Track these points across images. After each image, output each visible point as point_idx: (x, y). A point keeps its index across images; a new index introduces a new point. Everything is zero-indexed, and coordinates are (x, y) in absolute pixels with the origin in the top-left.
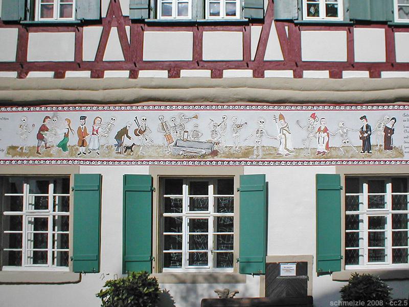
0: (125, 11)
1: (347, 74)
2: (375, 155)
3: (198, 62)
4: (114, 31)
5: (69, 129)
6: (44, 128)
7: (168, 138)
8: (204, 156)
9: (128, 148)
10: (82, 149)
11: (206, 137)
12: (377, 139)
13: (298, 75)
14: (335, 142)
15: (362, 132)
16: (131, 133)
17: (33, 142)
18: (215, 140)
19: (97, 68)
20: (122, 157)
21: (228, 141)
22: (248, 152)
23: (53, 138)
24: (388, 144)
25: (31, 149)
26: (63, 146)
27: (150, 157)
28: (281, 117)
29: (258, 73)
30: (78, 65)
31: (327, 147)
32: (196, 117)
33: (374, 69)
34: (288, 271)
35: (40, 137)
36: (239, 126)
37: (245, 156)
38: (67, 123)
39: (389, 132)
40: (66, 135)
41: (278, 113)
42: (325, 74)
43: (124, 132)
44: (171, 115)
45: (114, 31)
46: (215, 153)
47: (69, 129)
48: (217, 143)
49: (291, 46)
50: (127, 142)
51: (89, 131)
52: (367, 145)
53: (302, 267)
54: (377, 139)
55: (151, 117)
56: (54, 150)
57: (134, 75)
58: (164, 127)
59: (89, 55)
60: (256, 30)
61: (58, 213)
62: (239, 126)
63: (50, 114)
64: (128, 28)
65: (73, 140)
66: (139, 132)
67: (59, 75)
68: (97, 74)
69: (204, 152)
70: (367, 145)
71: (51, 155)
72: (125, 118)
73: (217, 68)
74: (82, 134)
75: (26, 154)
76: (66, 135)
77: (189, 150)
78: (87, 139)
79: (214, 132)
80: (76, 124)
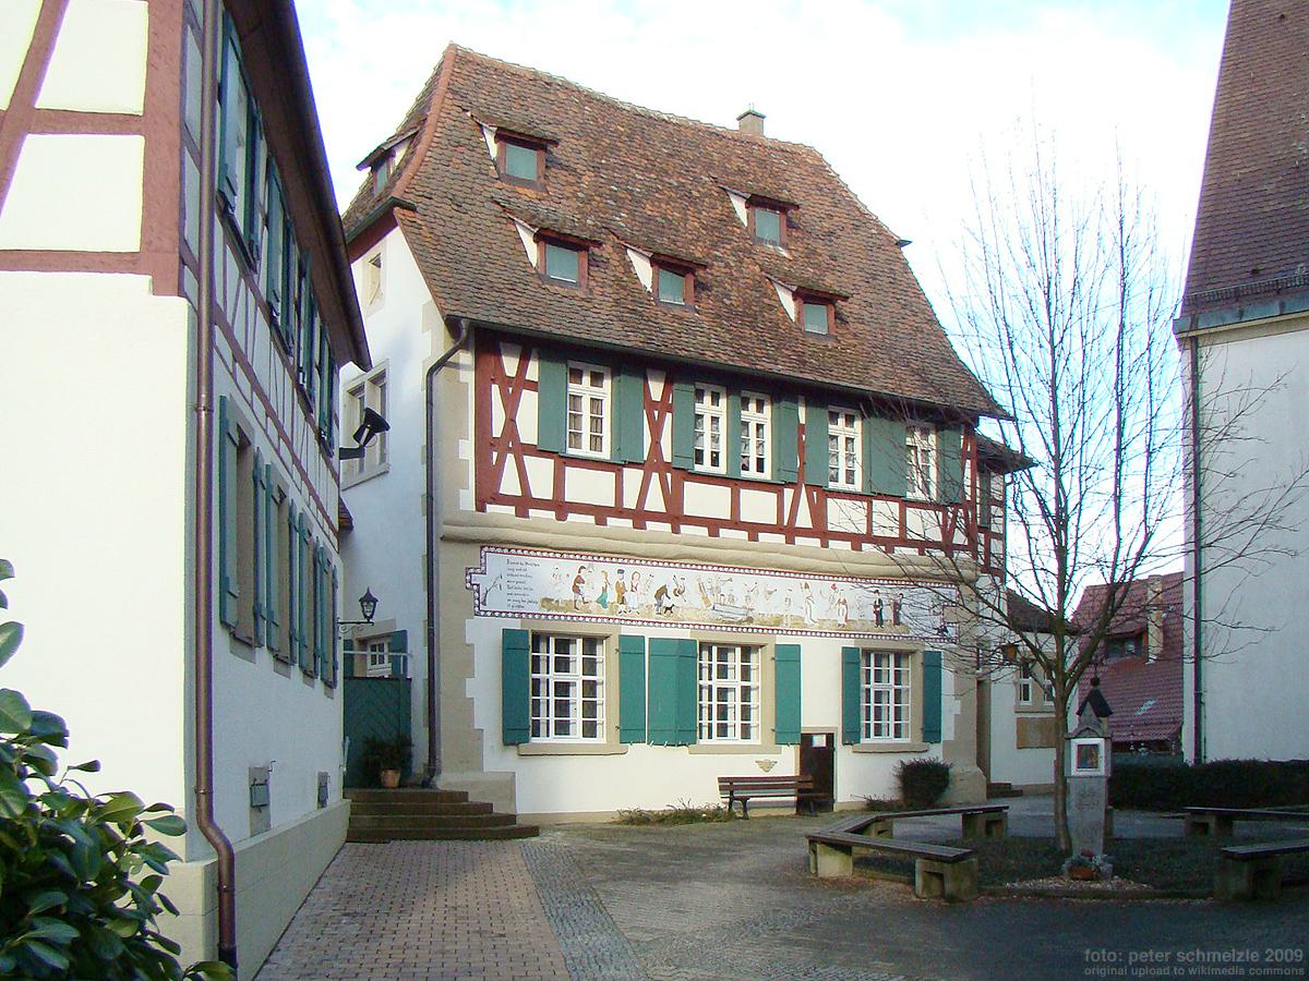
0: (667, 457)
1: (611, 521)
2: (888, 629)
3: (735, 523)
4: (655, 476)
5: (607, 583)
6: (579, 580)
7: (706, 599)
8: (740, 622)
9: (667, 609)
10: (622, 607)
11: (741, 602)
12: (888, 614)
13: (790, 541)
14: (853, 616)
15: (876, 606)
16: (670, 593)
17: (571, 596)
18: (749, 606)
19: (640, 517)
20: (661, 618)
21: (764, 609)
22: (779, 621)
23: (591, 592)
24: (897, 622)
25: (568, 603)
26: (602, 601)
27: (689, 619)
28: (807, 586)
29: (522, 512)
30: (619, 512)
31: (846, 620)
32: (731, 580)
33: (888, 544)
34: (819, 742)
35: (576, 590)
36: (770, 593)
37: (775, 626)
38: (604, 576)
39: (897, 607)
40: (604, 590)
41: (803, 582)
42: (847, 545)
43: (662, 592)
44: (708, 576)
45: (655, 476)
46: (750, 620)
47: (607, 583)
48: (752, 610)
49: (818, 513)
50: (666, 602)
51: (628, 587)
52: (880, 621)
53: (830, 738)
54: (888, 614)
55: (690, 578)
56: (593, 606)
57: (676, 530)
58: (701, 588)
59: (630, 502)
60: (789, 493)
61: (542, 675)
62: (770, 593)
63: (585, 564)
64: (669, 475)
65: (612, 596)
66: (678, 593)
67: (753, 538)
68: (638, 524)
69: (740, 618)
70: (880, 621)
71: (590, 612)
72: (663, 576)
73: (754, 529)
74: (621, 590)
75: (562, 608)
76: (604, 590)
77: (727, 615)
78: (625, 595)
79: (748, 598)
80: (614, 578)
